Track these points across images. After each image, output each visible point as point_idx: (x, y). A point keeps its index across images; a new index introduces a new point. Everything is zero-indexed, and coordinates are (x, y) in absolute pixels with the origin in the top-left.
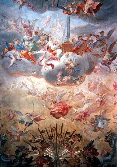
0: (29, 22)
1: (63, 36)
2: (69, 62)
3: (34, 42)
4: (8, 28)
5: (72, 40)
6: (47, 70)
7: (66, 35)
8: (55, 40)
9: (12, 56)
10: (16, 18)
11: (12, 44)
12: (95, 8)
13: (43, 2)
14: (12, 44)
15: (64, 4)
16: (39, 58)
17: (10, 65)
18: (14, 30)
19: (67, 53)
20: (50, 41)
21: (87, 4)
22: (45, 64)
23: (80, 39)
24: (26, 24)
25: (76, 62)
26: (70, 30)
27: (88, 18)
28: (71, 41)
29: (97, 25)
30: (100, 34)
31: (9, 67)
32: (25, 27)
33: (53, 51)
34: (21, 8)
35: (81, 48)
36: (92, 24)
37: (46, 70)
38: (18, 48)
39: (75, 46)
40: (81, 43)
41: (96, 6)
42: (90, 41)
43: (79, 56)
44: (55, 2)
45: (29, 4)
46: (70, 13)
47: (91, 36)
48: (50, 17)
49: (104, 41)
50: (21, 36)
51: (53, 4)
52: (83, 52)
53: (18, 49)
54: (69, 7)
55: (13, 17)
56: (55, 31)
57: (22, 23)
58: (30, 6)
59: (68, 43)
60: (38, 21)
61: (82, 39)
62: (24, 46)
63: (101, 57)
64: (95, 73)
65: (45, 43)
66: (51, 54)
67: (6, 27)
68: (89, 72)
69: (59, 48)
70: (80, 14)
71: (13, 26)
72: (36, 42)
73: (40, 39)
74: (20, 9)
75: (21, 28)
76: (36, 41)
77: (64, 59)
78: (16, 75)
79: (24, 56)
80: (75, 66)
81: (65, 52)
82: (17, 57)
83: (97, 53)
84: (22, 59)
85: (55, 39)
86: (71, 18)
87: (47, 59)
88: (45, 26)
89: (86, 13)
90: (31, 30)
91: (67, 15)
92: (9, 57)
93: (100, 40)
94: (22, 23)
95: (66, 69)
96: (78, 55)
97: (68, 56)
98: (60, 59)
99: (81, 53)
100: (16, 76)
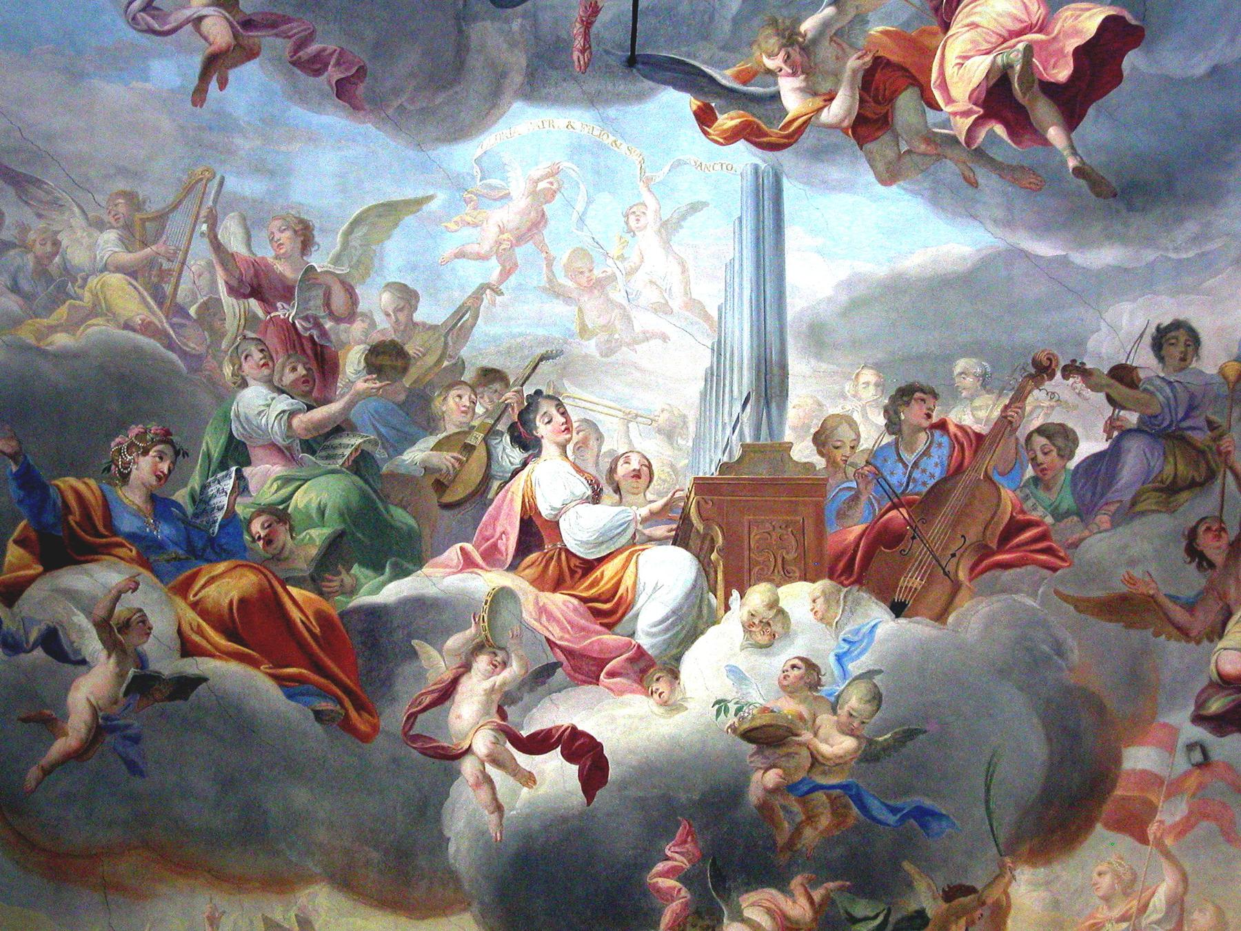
0: (305, 236)
1: (704, 395)
2: (789, 707)
3: (362, 464)
4: (54, 303)
5: (821, 440)
6: (509, 814)
7: (742, 381)
8: (613, 443)
9: (80, 630)
10: (157, 196)
11: (88, 487)
12: (1062, 73)
13: (462, 19)
14: (88, 487)
15: (705, 34)
16: (414, 654)
17: (59, 747)
18: (127, 326)
19: (758, 595)
20: (549, 449)
21: (974, 26)
22: (482, 743)
23: (912, 414)
24: (265, 252)
25: (876, 698)
26: (790, 315)
27: (988, 180)
28: (804, 452)
29: (1105, 256)
30: (1145, 360)
31: (33, 773)
32: (256, 292)
33: (589, 566)
34: (214, 85)
35: (936, 530)
36: (1045, 249)
37: (499, 808)
38: (164, 531)
39: (855, 498)
40: (934, 468)
41: (1072, 44)
42: (1040, 441)
43: (916, 629)
44: (602, 18)
45: (314, 48)
46: (775, 132)
47: (1048, 385)
48: (554, 173)
49: (1201, 438)
50: (205, 399)
51: (586, 35)
52: (962, 575)
53: (160, 546)
54: (770, 64)
55: (121, 185)
56: (609, 327)
57: (217, 247)
58: (315, 65)
59: (763, 473)
60: (409, 220)
61: (942, 426)
62: (231, 515)
63: (1183, 632)
64: (1125, 842)
65: (487, 478)
66: (558, 601)
67: (28, 298)
68: (1052, 831)
69: (661, 530)
70: (896, 137)
71: (116, 279)
72: (385, 469)
73: (430, 424)
74: (199, 95)
75: (211, 308)
76: (379, 454)
77: (733, 671)
78: (124, 867)
79: (231, 635)
80: (870, 754)
81: (739, 581)
82: (149, 647)
83: (1131, 581)
84: (200, 680)
85: (610, 426)
86: (786, 184)
87: (514, 670)
88: (494, 277)
89: (965, 124)
90: (328, 325)
91: (744, 155)
92: (53, 642)
93: (1150, 429)
94: (217, 247)
95: (754, 794)
96: (898, 609)
97: (777, 627)
98: (675, 674)
99: (930, 581)
100: (120, 888)
